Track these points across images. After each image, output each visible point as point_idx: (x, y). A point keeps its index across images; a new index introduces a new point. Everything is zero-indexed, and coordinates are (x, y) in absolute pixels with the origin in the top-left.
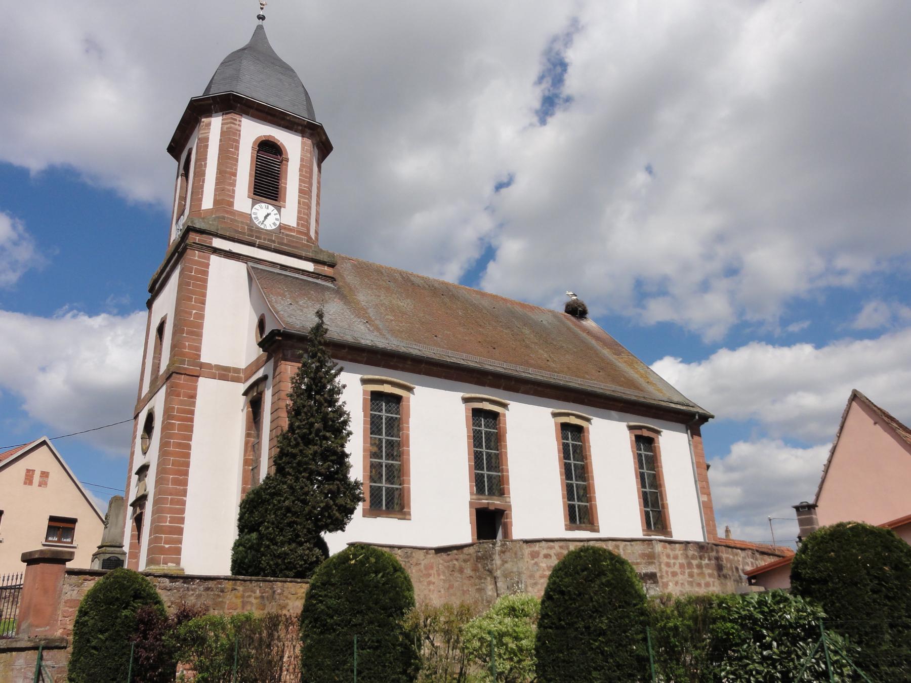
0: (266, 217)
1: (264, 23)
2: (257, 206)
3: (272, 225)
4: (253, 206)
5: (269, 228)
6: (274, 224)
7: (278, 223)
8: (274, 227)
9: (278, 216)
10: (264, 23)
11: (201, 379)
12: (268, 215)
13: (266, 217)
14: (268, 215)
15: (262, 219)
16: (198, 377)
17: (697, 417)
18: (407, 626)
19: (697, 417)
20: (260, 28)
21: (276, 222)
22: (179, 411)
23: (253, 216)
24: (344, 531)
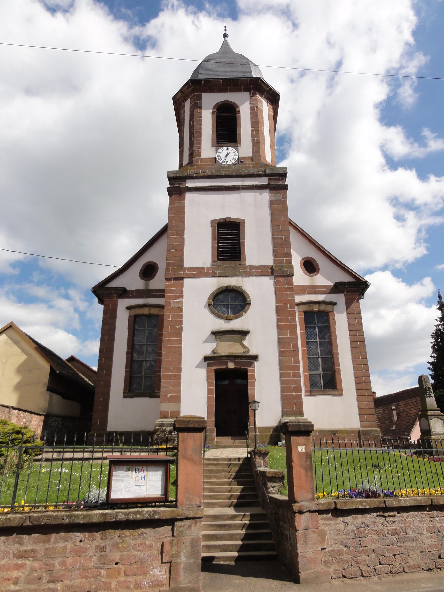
0: (226, 156)
1: (227, 39)
2: (220, 150)
3: (232, 160)
4: (217, 151)
5: (230, 163)
6: (234, 159)
7: (236, 158)
8: (234, 161)
9: (236, 153)
10: (227, 39)
11: (185, 280)
12: (228, 154)
13: (226, 156)
14: (228, 154)
15: (223, 158)
16: (182, 279)
17: (428, 509)
18: (422, 245)
19: (428, 509)
20: (225, 43)
21: (235, 154)
22: (343, 455)
23: (217, 158)
24: (255, 358)
